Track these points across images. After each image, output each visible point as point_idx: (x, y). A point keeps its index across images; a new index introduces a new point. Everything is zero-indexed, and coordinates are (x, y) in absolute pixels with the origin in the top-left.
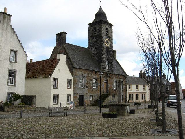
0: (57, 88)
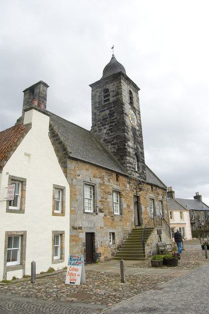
0: (21, 211)
